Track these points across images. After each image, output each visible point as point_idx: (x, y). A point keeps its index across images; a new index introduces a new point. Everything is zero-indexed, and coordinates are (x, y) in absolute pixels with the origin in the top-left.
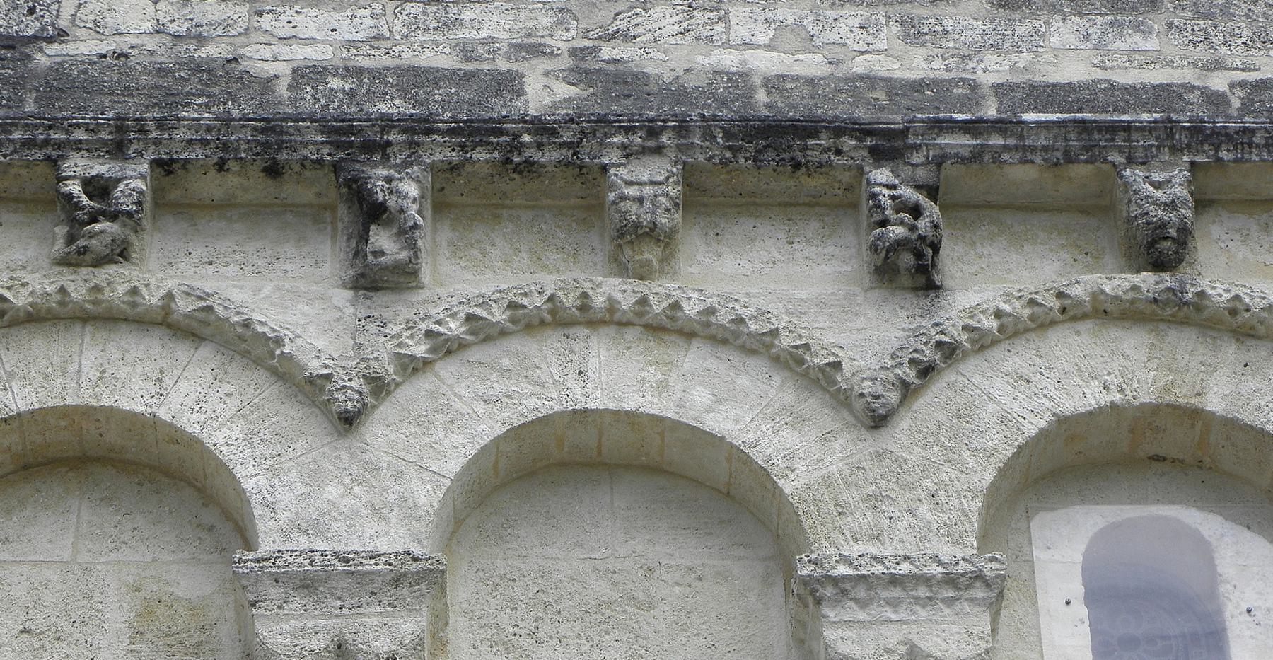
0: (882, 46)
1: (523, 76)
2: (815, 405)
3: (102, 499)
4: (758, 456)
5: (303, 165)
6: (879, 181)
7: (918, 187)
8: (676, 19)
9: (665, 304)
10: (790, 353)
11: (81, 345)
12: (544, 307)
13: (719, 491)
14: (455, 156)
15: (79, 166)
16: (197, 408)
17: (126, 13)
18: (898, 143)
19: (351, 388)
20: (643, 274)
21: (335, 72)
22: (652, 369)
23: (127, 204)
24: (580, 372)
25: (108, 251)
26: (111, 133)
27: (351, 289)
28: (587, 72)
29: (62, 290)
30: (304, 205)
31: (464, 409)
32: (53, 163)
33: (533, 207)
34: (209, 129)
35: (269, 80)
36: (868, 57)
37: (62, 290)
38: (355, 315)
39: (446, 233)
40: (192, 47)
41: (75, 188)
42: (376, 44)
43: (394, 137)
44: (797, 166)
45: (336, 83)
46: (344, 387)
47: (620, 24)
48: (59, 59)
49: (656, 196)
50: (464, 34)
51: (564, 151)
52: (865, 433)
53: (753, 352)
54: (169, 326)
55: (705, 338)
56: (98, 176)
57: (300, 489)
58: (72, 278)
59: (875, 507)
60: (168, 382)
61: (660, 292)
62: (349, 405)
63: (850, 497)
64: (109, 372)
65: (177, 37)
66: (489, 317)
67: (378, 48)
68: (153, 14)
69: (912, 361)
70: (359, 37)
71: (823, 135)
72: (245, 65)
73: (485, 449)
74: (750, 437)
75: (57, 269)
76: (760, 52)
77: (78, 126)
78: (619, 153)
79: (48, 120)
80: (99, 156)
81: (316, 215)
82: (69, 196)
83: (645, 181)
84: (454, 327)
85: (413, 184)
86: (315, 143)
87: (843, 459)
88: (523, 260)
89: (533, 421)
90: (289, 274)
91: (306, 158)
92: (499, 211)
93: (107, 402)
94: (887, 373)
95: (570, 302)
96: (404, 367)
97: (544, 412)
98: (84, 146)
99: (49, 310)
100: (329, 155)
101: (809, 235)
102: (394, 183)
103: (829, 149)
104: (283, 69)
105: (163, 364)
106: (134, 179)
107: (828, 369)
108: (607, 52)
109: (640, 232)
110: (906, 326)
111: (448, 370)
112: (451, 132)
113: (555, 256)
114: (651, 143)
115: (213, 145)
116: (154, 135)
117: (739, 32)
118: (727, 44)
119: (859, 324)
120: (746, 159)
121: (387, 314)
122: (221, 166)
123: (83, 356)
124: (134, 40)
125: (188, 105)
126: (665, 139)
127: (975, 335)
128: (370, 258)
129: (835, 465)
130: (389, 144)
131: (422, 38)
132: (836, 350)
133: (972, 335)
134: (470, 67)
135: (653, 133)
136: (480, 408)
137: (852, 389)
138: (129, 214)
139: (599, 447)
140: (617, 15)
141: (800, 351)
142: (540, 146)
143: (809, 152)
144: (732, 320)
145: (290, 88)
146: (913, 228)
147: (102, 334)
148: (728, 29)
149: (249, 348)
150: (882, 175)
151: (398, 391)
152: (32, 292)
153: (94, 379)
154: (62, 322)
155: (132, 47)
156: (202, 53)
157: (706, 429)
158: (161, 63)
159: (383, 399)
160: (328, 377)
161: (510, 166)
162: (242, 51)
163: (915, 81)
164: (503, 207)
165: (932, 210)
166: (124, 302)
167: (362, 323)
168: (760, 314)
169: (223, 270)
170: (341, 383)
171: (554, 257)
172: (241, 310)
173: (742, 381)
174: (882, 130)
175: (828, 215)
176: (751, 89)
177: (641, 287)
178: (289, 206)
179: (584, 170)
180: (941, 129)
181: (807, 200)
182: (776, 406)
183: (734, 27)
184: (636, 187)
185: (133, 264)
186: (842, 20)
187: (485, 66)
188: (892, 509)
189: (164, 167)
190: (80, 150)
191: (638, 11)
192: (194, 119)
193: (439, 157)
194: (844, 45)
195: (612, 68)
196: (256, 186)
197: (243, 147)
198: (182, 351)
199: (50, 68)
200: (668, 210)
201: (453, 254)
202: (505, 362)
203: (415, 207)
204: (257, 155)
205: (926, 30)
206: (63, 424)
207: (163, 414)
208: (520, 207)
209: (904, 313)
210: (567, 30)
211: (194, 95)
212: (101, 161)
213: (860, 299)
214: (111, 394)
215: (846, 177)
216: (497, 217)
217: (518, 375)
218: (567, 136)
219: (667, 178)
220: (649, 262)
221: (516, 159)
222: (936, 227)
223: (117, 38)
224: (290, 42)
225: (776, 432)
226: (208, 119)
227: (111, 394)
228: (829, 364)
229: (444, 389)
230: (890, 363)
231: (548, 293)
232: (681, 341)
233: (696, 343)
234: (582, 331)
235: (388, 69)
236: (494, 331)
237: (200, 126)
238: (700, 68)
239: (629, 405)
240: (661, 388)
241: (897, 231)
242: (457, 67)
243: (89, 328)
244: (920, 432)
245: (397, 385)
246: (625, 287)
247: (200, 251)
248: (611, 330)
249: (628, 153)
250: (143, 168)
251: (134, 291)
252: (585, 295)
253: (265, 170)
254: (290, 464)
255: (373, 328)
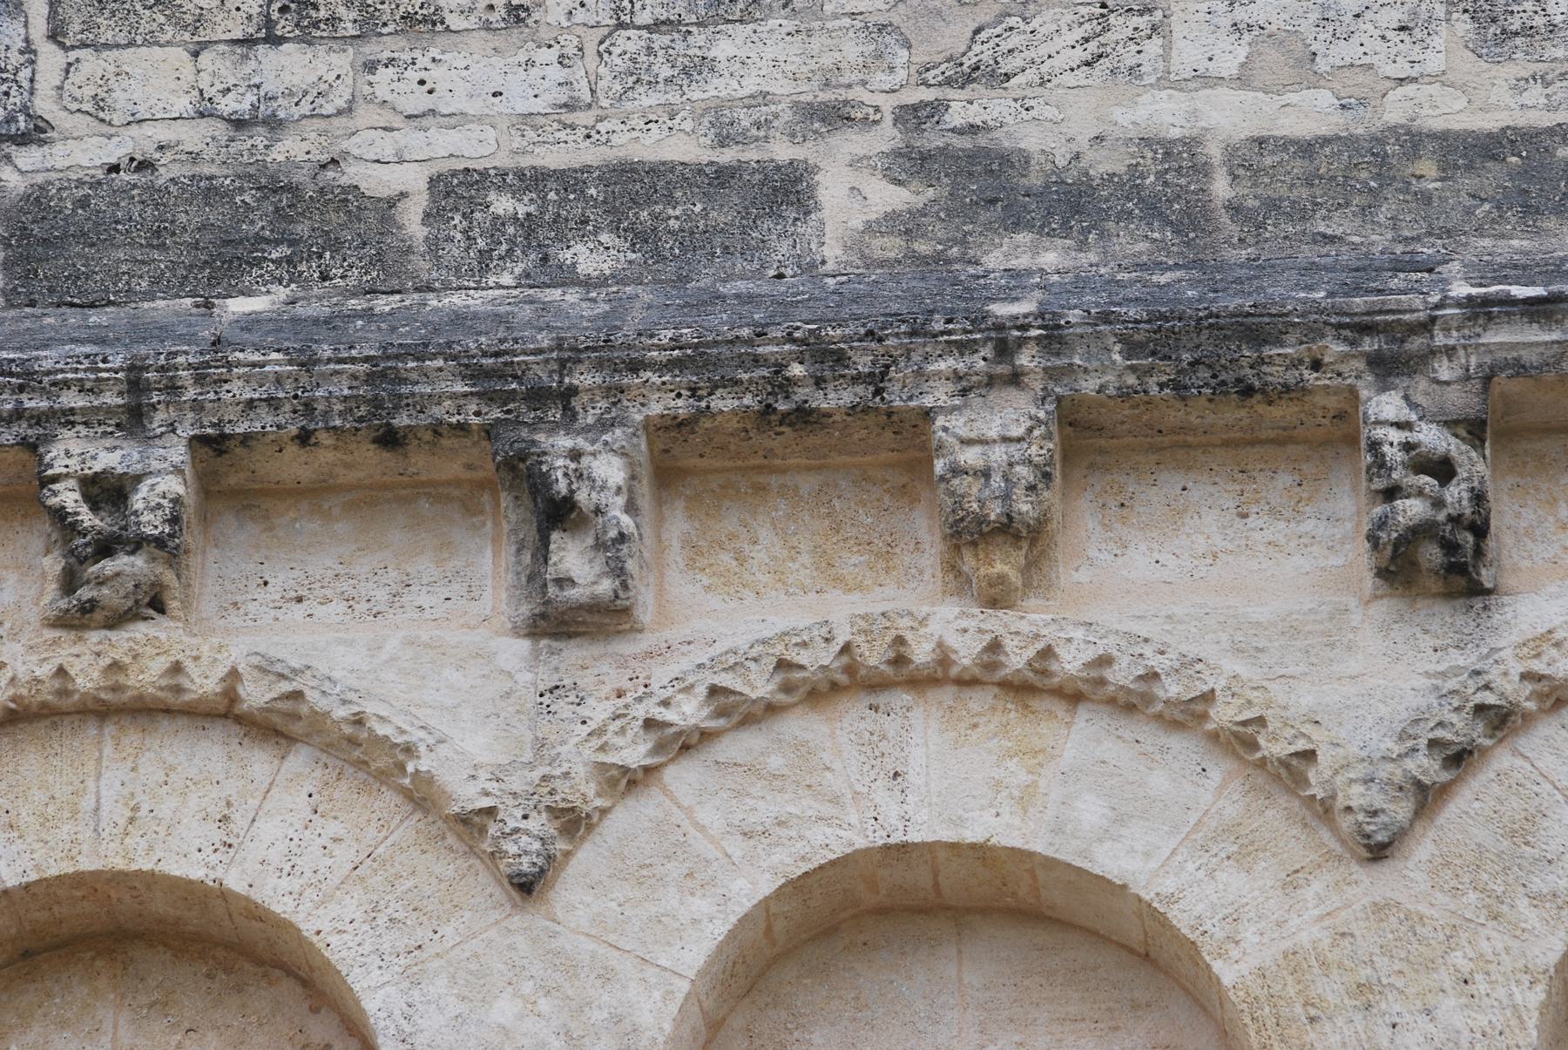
0: (1434, 63)
1: (815, 170)
2: (1275, 818)
3: (151, 1006)
4: (1181, 918)
5: (435, 432)
6: (1383, 416)
7: (1450, 424)
8: (1079, 33)
9: (1031, 652)
10: (1236, 735)
11: (99, 760)
12: (836, 664)
13: (1131, 951)
14: (682, 407)
15: (73, 453)
16: (287, 868)
17: (146, 79)
18: (1416, 343)
19: (527, 833)
20: (996, 598)
21: (501, 180)
22: (1012, 764)
23: (152, 524)
24: (896, 774)
25: (130, 603)
26: (120, 394)
27: (528, 635)
28: (925, 157)
29: (61, 672)
30: (448, 483)
31: (711, 852)
32: (31, 447)
33: (819, 468)
34: (279, 380)
35: (392, 203)
36: (1410, 89)
37: (61, 672)
38: (535, 684)
39: (678, 525)
40: (260, 141)
41: (68, 497)
42: (569, 118)
43: (584, 378)
44: (1247, 391)
45: (503, 204)
46: (516, 830)
47: (983, 52)
48: (40, 179)
49: (1011, 465)
50: (717, 88)
51: (860, 389)
52: (1360, 873)
53: (1176, 725)
54: (240, 719)
55: (1101, 702)
56: (104, 472)
57: (454, 1007)
58: (75, 650)
59: (1368, 1007)
60: (240, 821)
61: (1023, 630)
62: (525, 868)
63: (1330, 989)
64: (145, 808)
65: (238, 124)
66: (746, 690)
67: (573, 127)
68: (191, 78)
69: (1433, 743)
70: (539, 106)
71: (1291, 338)
72: (352, 174)
73: (744, 920)
74: (1168, 885)
75: (51, 634)
76: (1222, 92)
77: (66, 384)
78: (950, 387)
79: (18, 376)
80: (105, 434)
81: (465, 499)
82: (59, 514)
83: (991, 434)
84: (689, 712)
85: (617, 462)
86: (454, 396)
87: (1321, 918)
88: (802, 568)
89: (821, 867)
90: (427, 614)
91: (440, 422)
92: (761, 479)
93: (145, 865)
94: (1390, 767)
95: (874, 656)
96: (612, 783)
97: (838, 851)
98: (78, 418)
99: (44, 705)
100: (478, 414)
101: (1275, 499)
102: (585, 461)
103: (1301, 361)
104: (414, 179)
105: (231, 788)
106: (163, 478)
107: (1294, 762)
108: (957, 115)
109: (985, 529)
110: (1432, 667)
111: (683, 777)
112: (670, 365)
113: (855, 559)
114: (1002, 369)
115: (287, 407)
116: (190, 394)
117: (1187, 56)
118: (1165, 81)
119: (1354, 665)
120: (1162, 386)
121: (586, 680)
122: (304, 438)
123: (103, 782)
124: (163, 133)
125: (258, 263)
126: (1025, 359)
127: (1543, 687)
128: (552, 590)
129: (1307, 932)
130: (573, 391)
131: (646, 102)
132: (1307, 729)
133: (1538, 687)
134: (727, 156)
135: (1004, 350)
136: (736, 847)
137: (1333, 797)
138: (159, 542)
139: (936, 885)
140: (977, 31)
141: (1250, 730)
142: (819, 382)
143: (1265, 368)
144: (1140, 677)
145: (427, 217)
146: (1438, 503)
147: (132, 738)
148: (1167, 47)
149: (362, 755)
150: (1387, 405)
151: (606, 822)
152: (13, 679)
153: (122, 822)
154: (67, 720)
155: (161, 148)
156: (277, 154)
157: (1097, 871)
158: (210, 178)
159: (583, 839)
160: (490, 812)
161: (773, 417)
162: (345, 144)
163: (1490, 135)
164: (773, 470)
165: (1472, 464)
166: (161, 689)
167: (546, 700)
168: (1190, 663)
169: (320, 611)
170: (512, 824)
171: (852, 562)
172: (351, 696)
173: (1159, 781)
174: (1387, 323)
175: (1308, 459)
176: (1202, 170)
177: (998, 622)
178: (423, 484)
179: (895, 418)
180: (1490, 317)
181: (1272, 434)
182: (1214, 824)
183: (1179, 44)
184: (978, 449)
185: (173, 618)
186: (1369, 15)
187: (751, 155)
188: (1397, 1008)
189: (212, 446)
190: (73, 424)
191: (1012, 21)
192: (254, 365)
193: (656, 409)
194: (1370, 67)
195: (965, 143)
196: (370, 461)
197: (338, 407)
198: (260, 762)
199: (26, 197)
200: (1031, 488)
201: (691, 564)
202: (775, 762)
203: (620, 501)
204: (361, 420)
205: (1516, 26)
206: (79, 894)
207: (235, 882)
208: (798, 469)
209: (1427, 642)
210: (892, 69)
211: (268, 241)
212: (109, 442)
213: (1356, 618)
214: (151, 848)
215: (1332, 403)
216: (760, 489)
217: (798, 783)
218: (863, 363)
219: (1030, 430)
220: (1002, 579)
221: (782, 406)
222: (1478, 498)
223: (134, 130)
224: (425, 122)
225: (1211, 874)
226: (277, 362)
227: (151, 848)
228: (1296, 754)
229: (678, 816)
230: (1397, 749)
231: (840, 641)
232: (1059, 708)
233: (1083, 712)
234: (901, 698)
235: (587, 169)
236: (758, 710)
237: (265, 376)
238: (1118, 133)
239: (972, 834)
240: (1026, 799)
241: (1412, 509)
242: (705, 160)
243: (110, 729)
244: (1448, 864)
245: (604, 812)
246: (964, 623)
247: (282, 579)
248: (947, 694)
249: (965, 387)
250: (177, 452)
251: (177, 668)
252: (900, 641)
253: (376, 441)
254: (436, 964)
255: (563, 708)
